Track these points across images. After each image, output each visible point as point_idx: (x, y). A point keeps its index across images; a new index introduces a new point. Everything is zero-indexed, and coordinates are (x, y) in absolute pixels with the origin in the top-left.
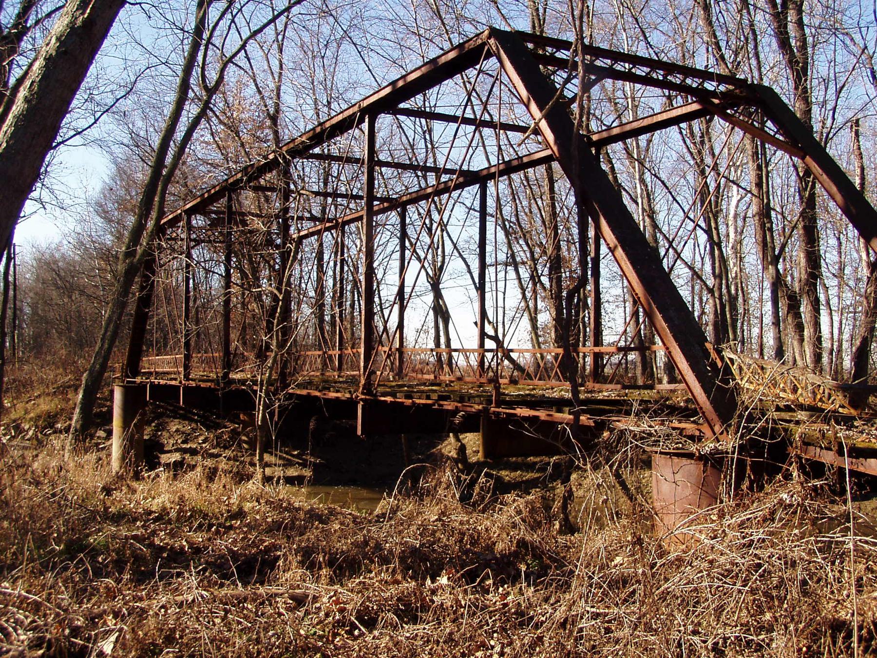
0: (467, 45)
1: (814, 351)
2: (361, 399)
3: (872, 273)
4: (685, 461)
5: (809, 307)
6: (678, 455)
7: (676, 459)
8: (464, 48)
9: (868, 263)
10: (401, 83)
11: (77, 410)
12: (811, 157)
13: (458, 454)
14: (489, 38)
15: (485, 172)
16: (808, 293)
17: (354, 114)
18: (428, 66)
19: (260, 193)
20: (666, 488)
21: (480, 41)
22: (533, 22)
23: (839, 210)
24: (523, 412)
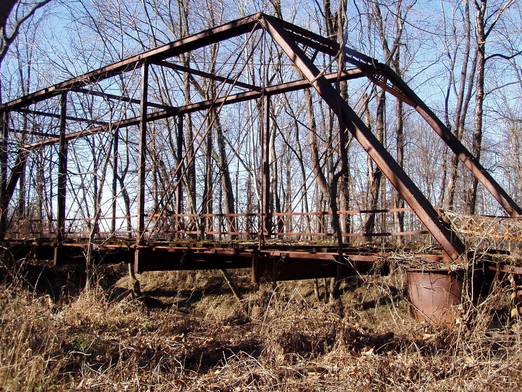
0: (239, 22)
1: (346, 223)
2: (138, 249)
3: (374, 180)
4: (439, 276)
5: (344, 198)
6: (434, 272)
7: (433, 275)
8: (237, 24)
9: (372, 174)
10: (178, 44)
11: (117, 246)
12: (420, 106)
13: (135, 287)
14: (260, 18)
15: (183, 109)
16: (343, 190)
17: (135, 62)
18: (203, 34)
19: (372, 83)
20: (425, 293)
21: (251, 20)
22: (341, 6)
23: (438, 136)
24: (277, 253)
